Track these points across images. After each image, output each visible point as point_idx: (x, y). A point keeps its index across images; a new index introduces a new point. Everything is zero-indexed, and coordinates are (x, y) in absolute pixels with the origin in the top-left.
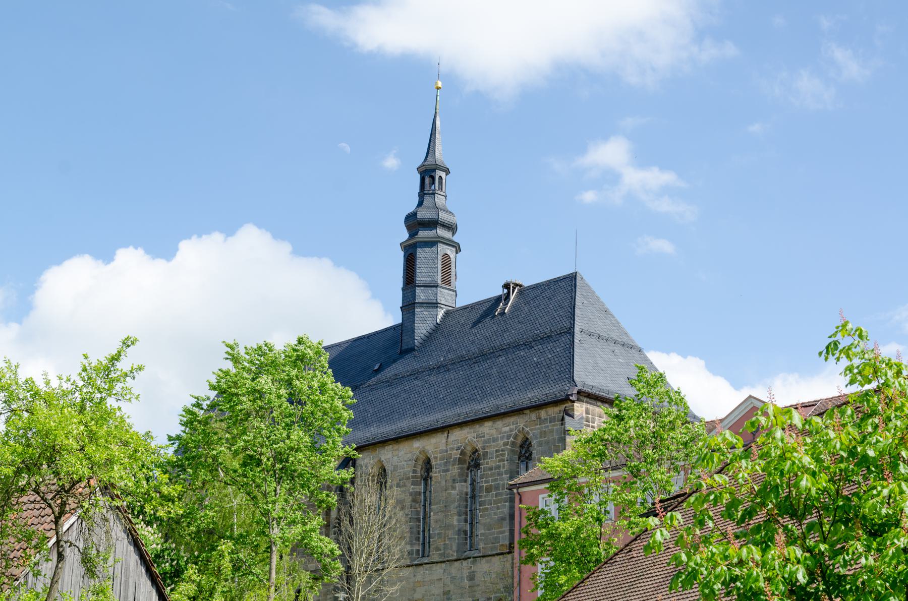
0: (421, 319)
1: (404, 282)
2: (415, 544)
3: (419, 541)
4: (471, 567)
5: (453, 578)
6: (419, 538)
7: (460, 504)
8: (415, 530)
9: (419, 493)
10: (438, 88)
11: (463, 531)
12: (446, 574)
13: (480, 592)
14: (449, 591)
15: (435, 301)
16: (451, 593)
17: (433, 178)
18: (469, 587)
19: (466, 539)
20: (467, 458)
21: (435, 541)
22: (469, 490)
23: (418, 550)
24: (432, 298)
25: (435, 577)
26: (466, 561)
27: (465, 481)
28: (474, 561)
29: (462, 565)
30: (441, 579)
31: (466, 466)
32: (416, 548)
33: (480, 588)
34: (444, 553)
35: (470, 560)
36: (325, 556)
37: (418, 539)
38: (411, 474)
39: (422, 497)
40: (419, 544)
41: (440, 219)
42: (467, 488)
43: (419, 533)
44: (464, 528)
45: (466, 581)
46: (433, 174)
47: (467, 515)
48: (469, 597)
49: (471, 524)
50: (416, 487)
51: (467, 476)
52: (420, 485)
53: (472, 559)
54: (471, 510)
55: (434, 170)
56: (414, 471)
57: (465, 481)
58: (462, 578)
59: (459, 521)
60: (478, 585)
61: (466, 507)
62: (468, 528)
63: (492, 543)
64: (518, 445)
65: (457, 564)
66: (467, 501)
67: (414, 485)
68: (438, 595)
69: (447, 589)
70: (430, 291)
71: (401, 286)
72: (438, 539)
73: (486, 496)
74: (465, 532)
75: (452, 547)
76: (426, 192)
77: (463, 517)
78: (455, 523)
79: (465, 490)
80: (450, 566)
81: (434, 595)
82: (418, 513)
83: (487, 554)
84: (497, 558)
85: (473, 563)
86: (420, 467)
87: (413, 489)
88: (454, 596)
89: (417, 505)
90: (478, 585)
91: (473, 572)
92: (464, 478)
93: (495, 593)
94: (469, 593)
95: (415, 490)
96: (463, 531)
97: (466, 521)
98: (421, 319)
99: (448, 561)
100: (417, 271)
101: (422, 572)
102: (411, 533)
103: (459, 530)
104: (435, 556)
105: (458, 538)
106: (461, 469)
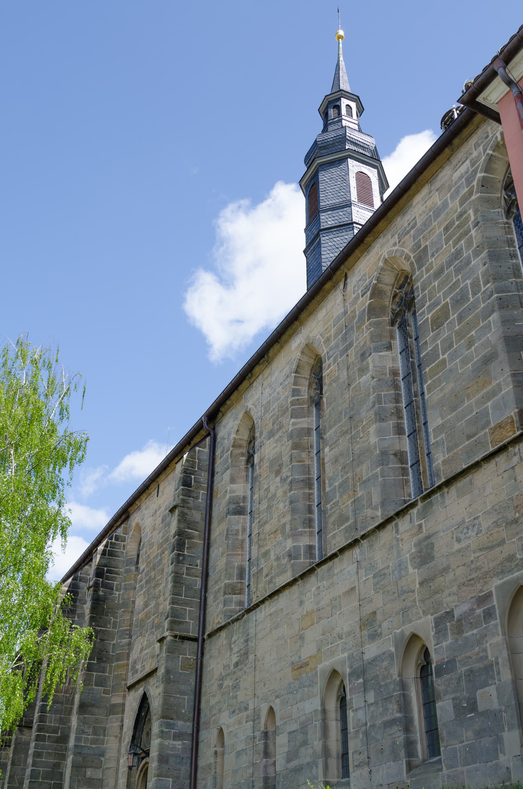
0: (330, 248)
1: (306, 222)
2: (301, 534)
3: (310, 527)
4: (420, 526)
5: (380, 575)
6: (311, 520)
7: (379, 396)
8: (301, 505)
9: (308, 432)
10: (340, 37)
11: (395, 455)
12: (362, 572)
13: (455, 589)
14: (374, 613)
15: (350, 222)
16: (379, 617)
17: (338, 108)
18: (421, 584)
19: (404, 472)
20: (387, 302)
21: (336, 504)
22: (400, 364)
23: (310, 548)
24: (346, 220)
25: (341, 589)
26: (407, 517)
27: (389, 347)
28: (425, 508)
29: (397, 531)
30: (353, 589)
31: (387, 318)
32: (304, 541)
33: (450, 576)
34: (355, 522)
35: (415, 511)
36: (80, 580)
37: (309, 523)
38: (290, 399)
39: (314, 437)
40: (311, 534)
41: (347, 134)
42: (394, 360)
43: (310, 511)
44: (397, 447)
45: (411, 570)
46: (338, 103)
47: (400, 418)
48: (425, 613)
49: (414, 433)
50: (299, 420)
51: (392, 337)
52: (309, 414)
53: (420, 505)
54: (409, 404)
55: (339, 99)
56: (295, 392)
57: (389, 347)
58: (401, 567)
59: (380, 432)
60: (446, 570)
61: (397, 399)
62: (406, 445)
63: (469, 437)
64: (500, 185)
65: (386, 535)
66: (396, 387)
67: (296, 417)
68: (349, 634)
69: (368, 609)
70: (341, 213)
71: (304, 226)
72: (341, 496)
73: (435, 339)
74: (400, 456)
75: (370, 499)
76: (360, 227)
77: (391, 423)
78: (373, 439)
79: (389, 365)
80: (371, 546)
81: (340, 637)
82: (307, 469)
83: (459, 470)
84: (489, 468)
85: (423, 515)
86: (307, 383)
87: (294, 424)
88: (385, 625)
89: (304, 455)
90: (446, 570)
91: (428, 537)
92: (385, 341)
93: (503, 572)
94: (423, 601)
95: (297, 426)
96: (395, 455)
97: (399, 430)
98: (330, 248)
99: (363, 537)
100: (321, 195)
101: (314, 589)
102: (293, 511)
103: (384, 453)
104: (338, 539)
105: (382, 471)
106: (377, 324)
